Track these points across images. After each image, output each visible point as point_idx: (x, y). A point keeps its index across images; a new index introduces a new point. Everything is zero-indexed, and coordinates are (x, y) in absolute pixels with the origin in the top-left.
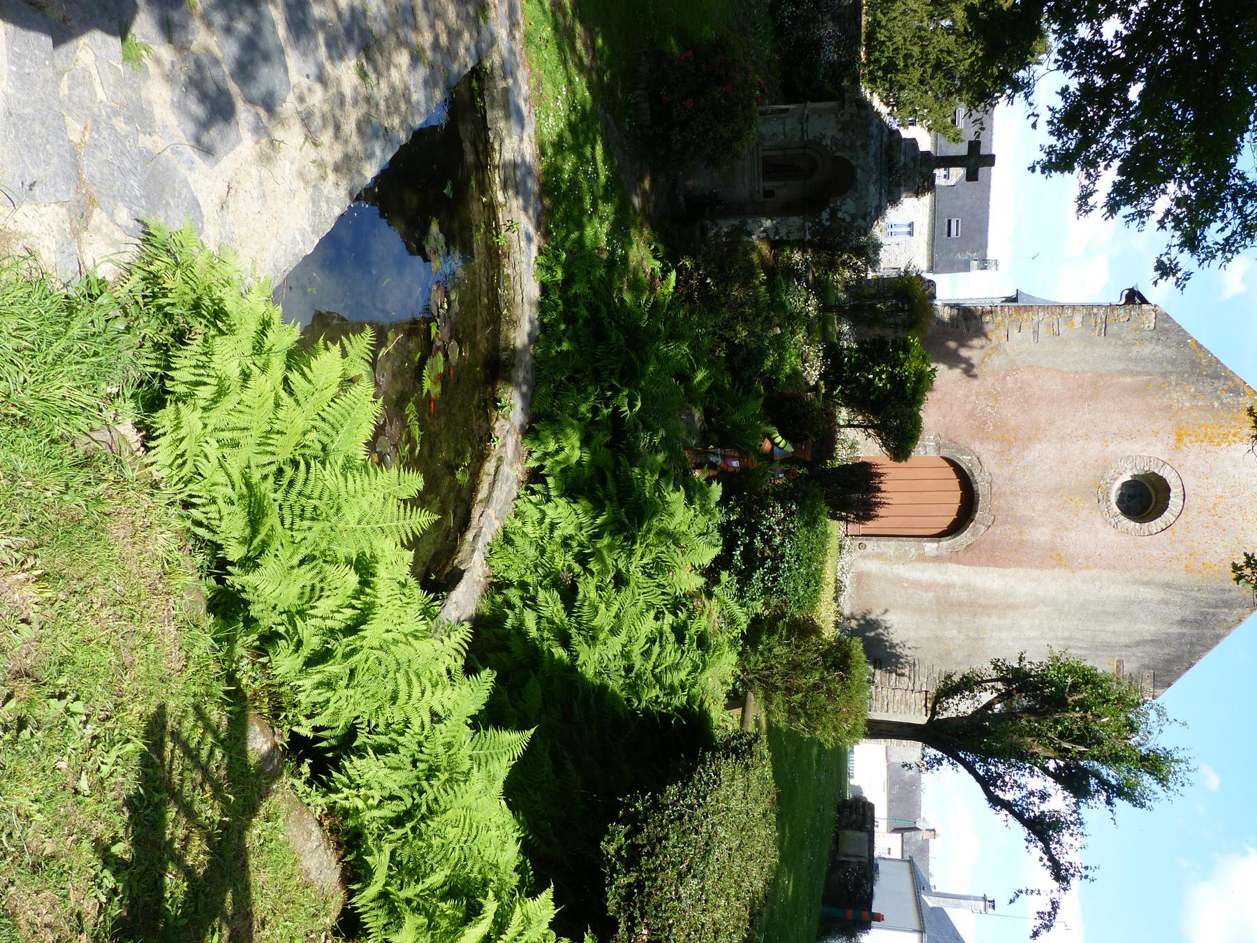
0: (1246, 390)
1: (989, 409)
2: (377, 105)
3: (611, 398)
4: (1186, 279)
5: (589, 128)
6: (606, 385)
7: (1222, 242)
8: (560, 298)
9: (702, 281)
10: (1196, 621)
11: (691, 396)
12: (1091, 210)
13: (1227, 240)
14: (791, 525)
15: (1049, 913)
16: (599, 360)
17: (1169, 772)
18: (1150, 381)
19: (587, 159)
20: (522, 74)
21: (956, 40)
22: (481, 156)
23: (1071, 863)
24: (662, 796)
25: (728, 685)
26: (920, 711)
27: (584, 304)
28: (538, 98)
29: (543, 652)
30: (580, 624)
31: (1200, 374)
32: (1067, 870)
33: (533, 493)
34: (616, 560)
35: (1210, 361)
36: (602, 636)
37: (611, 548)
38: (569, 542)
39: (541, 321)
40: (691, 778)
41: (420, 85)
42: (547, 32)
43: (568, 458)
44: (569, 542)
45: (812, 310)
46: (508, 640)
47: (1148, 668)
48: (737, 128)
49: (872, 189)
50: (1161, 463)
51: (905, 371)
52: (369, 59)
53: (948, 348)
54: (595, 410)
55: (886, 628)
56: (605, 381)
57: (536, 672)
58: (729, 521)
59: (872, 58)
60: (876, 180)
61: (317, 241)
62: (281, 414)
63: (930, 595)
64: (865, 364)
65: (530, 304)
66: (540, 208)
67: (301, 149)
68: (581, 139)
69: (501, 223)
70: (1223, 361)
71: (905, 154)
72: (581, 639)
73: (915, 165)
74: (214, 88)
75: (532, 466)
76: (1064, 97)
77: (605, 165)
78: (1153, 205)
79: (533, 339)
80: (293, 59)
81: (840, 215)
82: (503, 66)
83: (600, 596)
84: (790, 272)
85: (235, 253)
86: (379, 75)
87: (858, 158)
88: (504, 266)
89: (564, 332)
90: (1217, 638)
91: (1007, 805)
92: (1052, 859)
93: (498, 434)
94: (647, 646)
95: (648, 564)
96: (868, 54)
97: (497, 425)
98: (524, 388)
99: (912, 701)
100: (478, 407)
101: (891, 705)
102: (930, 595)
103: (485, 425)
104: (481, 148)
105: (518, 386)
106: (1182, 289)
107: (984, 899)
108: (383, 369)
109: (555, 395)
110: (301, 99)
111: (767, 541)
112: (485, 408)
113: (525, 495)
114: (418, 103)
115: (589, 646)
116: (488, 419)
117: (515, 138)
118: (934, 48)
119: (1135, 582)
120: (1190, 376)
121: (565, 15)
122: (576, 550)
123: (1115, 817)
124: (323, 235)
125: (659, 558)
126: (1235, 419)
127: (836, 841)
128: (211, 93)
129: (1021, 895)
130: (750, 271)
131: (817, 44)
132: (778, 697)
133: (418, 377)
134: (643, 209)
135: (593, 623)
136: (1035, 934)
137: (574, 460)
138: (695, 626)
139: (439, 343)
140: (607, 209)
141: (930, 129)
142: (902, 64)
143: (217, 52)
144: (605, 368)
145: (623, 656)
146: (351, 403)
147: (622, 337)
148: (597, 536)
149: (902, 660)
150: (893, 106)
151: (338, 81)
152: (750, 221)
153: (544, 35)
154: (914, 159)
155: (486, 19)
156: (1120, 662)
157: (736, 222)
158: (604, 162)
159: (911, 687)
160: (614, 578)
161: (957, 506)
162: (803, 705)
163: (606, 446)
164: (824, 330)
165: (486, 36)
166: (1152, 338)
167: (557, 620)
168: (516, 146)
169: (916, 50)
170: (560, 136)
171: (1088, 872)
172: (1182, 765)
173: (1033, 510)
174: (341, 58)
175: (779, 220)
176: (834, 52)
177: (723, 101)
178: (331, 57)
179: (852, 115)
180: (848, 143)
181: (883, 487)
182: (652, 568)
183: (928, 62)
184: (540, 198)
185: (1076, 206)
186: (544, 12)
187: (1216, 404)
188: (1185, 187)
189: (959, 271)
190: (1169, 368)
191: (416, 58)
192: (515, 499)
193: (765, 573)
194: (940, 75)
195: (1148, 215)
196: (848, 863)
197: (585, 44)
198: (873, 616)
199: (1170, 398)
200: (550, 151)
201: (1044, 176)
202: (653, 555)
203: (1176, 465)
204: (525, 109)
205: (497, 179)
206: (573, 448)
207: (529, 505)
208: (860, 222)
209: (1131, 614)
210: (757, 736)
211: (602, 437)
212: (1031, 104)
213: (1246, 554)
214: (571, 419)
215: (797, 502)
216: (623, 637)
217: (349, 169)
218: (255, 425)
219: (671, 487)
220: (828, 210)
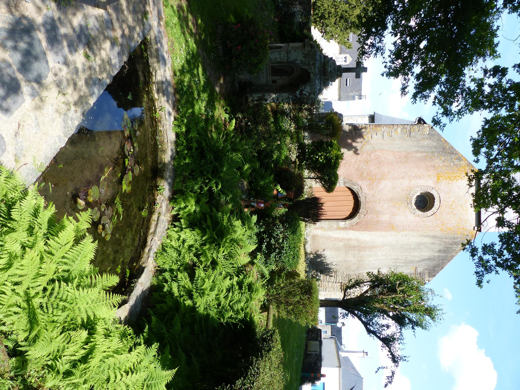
0: (463, 158)
1: (364, 167)
2: (95, 69)
3: (208, 183)
4: (444, 127)
5: (195, 61)
6: (206, 178)
7: (457, 111)
8: (184, 139)
9: (246, 124)
10: (445, 250)
11: (243, 175)
12: (406, 94)
13: (459, 110)
14: (286, 234)
15: (391, 376)
16: (202, 167)
17: (435, 314)
18: (427, 155)
19: (195, 74)
20: (164, 41)
21: (349, 7)
22: (147, 78)
23: (399, 355)
24: (235, 386)
25: (262, 302)
26: (339, 290)
27: (195, 141)
28: (172, 50)
29: (181, 303)
30: (197, 287)
31: (446, 152)
32: (397, 358)
33: (175, 226)
34: (212, 254)
35: (450, 147)
36: (207, 292)
37: (209, 249)
38: (191, 248)
39: (176, 150)
40: (247, 375)
41: (116, 55)
42: (175, 20)
43: (190, 210)
44: (191, 248)
45: (293, 129)
46: (165, 298)
47: (426, 269)
48: (260, 58)
49: (317, 82)
50: (431, 188)
51: (331, 155)
52: (91, 49)
53: (348, 142)
54: (201, 188)
55: (325, 257)
56: (205, 176)
57: (178, 312)
58: (260, 231)
59: (315, 13)
60: (319, 78)
61: (67, 140)
62: (43, 266)
63: (342, 243)
64: (315, 152)
65: (172, 143)
66: (174, 99)
67: (57, 98)
68: (192, 66)
69: (157, 107)
70: (454, 147)
71: (330, 67)
72: (197, 294)
73: (335, 72)
74: (9, 78)
75: (174, 214)
76: (395, 45)
77: (203, 76)
78: (430, 93)
79: (173, 158)
80: (51, 57)
81: (304, 92)
82: (156, 38)
83: (205, 274)
84: (283, 113)
85: (24, 156)
86: (95, 55)
87: (311, 69)
88: (159, 126)
89: (187, 154)
90: (452, 257)
91: (374, 333)
92: (392, 354)
93: (158, 202)
94: (227, 294)
95: (226, 255)
96: (314, 12)
97: (158, 198)
98: (169, 180)
99: (336, 286)
100: (149, 190)
101: (327, 288)
102: (342, 243)
103: (152, 198)
104: (146, 74)
105: (167, 180)
106: (442, 131)
107: (364, 352)
108: (103, 186)
109: (183, 181)
110: (56, 75)
111: (277, 241)
112: (152, 190)
113: (171, 227)
114: (115, 64)
115: (201, 297)
116: (154, 195)
117: (162, 70)
118: (340, 10)
119: (422, 236)
120: (442, 153)
121: (183, 11)
122: (194, 252)
123: (415, 334)
124: (69, 136)
125: (230, 252)
126: (459, 170)
127: (306, 346)
128: (7, 81)
129: (380, 369)
130: (267, 118)
131: (293, 15)
132: (282, 306)
133: (121, 184)
134: (220, 92)
135: (203, 288)
136: (386, 386)
137: (192, 211)
138: (247, 281)
139: (129, 167)
140: (205, 96)
141: (339, 43)
142: (327, 16)
143: (10, 60)
144: (205, 170)
145: (216, 299)
146: (81, 248)
147: (212, 156)
148: (203, 245)
149: (331, 270)
150: (324, 33)
151: (75, 62)
152: (266, 95)
153: (174, 22)
154: (334, 69)
155: (147, 19)
156: (416, 268)
157: (261, 95)
158: (203, 75)
159: (335, 281)
160: (211, 263)
161: (352, 207)
162: (293, 310)
163: (207, 203)
164: (298, 137)
165: (147, 27)
166: (428, 138)
167: (187, 286)
168: (162, 74)
169: (333, 10)
170: (183, 67)
171: (406, 358)
172: (440, 312)
173: (383, 208)
174: (76, 51)
175: (278, 94)
176: (300, 18)
177: (254, 47)
178: (71, 52)
179: (308, 51)
180: (307, 63)
181: (323, 208)
182: (228, 256)
183: (338, 16)
184: (174, 94)
185: (401, 92)
186: (174, 11)
187: (452, 164)
188: (442, 87)
189: (351, 100)
190: (435, 150)
191: (113, 43)
192: (167, 230)
193: (276, 254)
194: (342, 21)
195: (428, 98)
196: (312, 354)
197: (193, 23)
198: (319, 253)
199: (435, 162)
200: (178, 74)
201: (387, 78)
202: (228, 251)
203: (437, 189)
204: (166, 56)
205: (155, 88)
206: (192, 206)
207: (173, 232)
208: (312, 96)
209: (420, 249)
210: (274, 331)
211: (204, 200)
212: (384, 58)
213: (467, 240)
214: (191, 193)
215: (289, 223)
216: (216, 292)
217: (82, 103)
218: (30, 273)
219: (235, 219)
220: (299, 91)
